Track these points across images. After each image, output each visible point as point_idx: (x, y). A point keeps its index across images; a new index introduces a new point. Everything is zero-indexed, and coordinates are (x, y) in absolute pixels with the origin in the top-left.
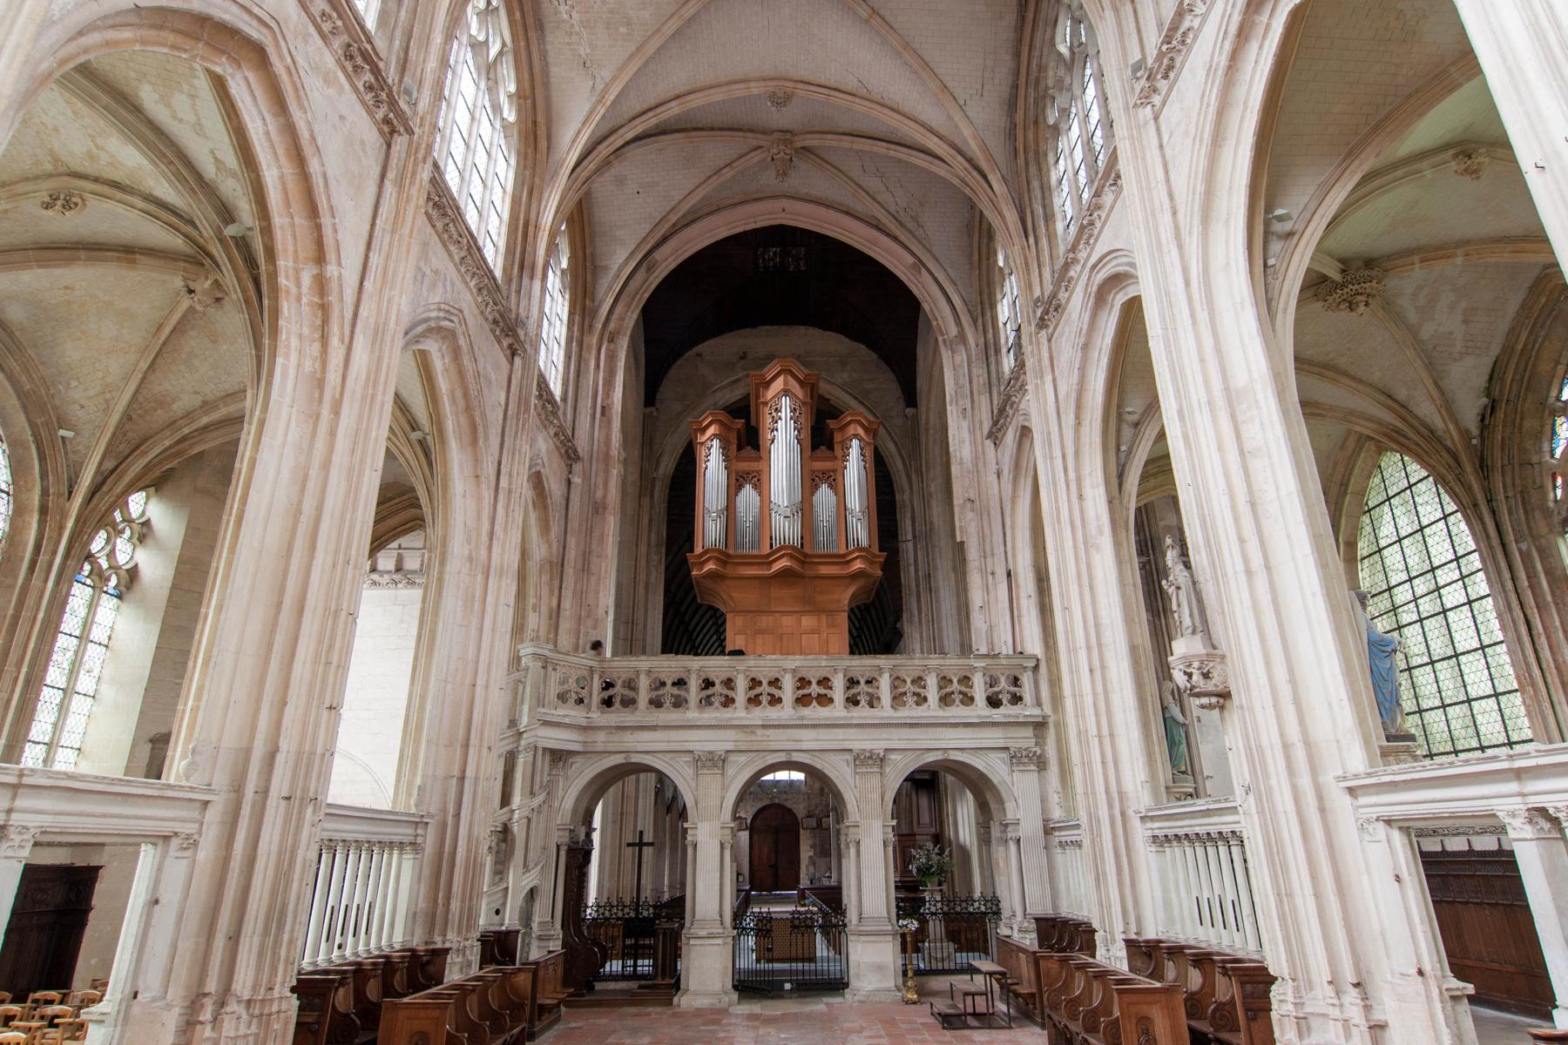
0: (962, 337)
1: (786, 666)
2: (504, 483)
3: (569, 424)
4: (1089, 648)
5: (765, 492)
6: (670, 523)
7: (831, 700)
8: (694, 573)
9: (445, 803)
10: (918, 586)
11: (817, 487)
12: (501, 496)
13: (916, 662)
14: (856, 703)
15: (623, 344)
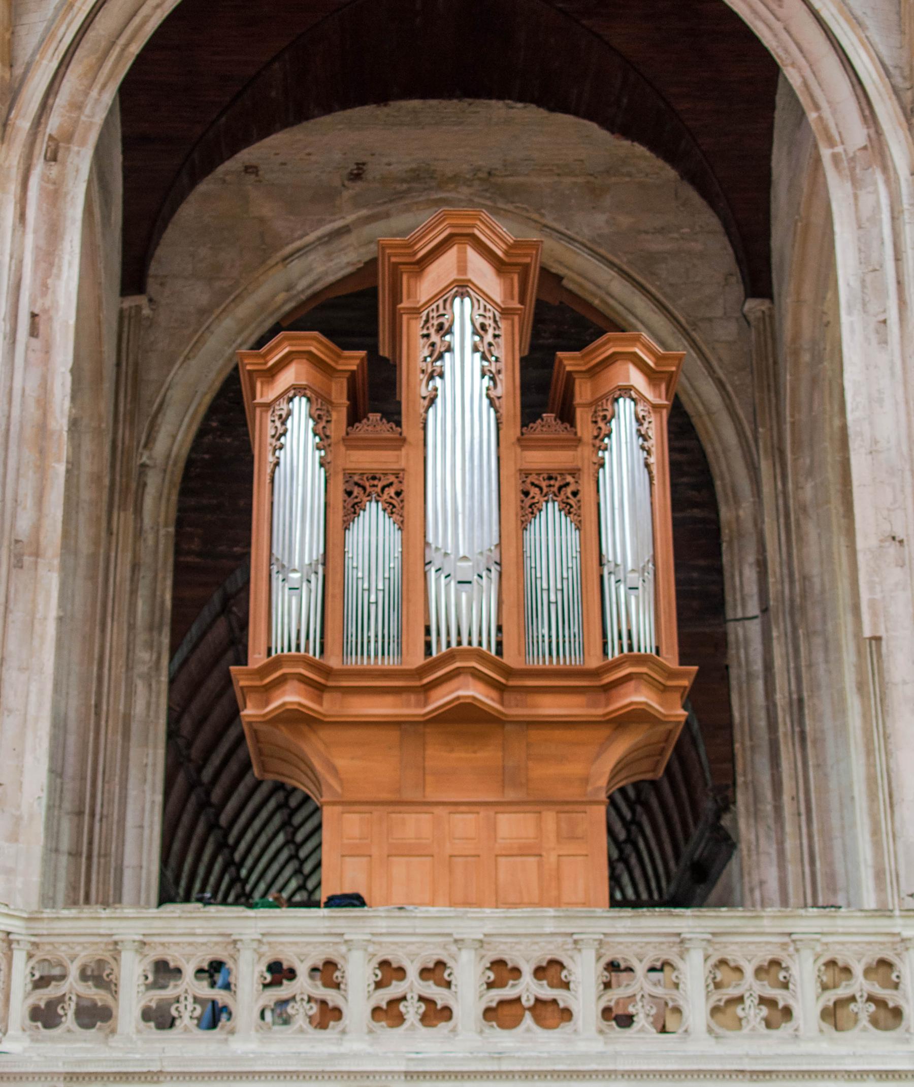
0: (877, 146)
1: (466, 934)
5: (414, 520)
6: (183, 573)
7: (567, 1014)
8: (250, 712)
10: (772, 726)
13: (767, 924)
14: (626, 1021)
15: (80, 162)
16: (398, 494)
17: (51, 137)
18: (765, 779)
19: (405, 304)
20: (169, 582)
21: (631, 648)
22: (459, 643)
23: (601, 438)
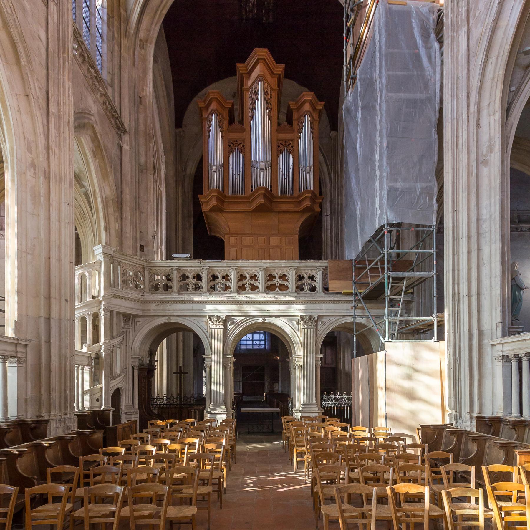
2: (53, 108)
3: (117, 104)
4: (469, 238)
7: (287, 288)
9: (38, 334)
11: (281, 152)
12: (52, 119)
15: (151, 50)
16: (243, 146)
17: (141, 40)
18: (329, 253)
19: (244, 87)
20: (192, 206)
21: (307, 188)
22: (260, 185)
23: (300, 130)
